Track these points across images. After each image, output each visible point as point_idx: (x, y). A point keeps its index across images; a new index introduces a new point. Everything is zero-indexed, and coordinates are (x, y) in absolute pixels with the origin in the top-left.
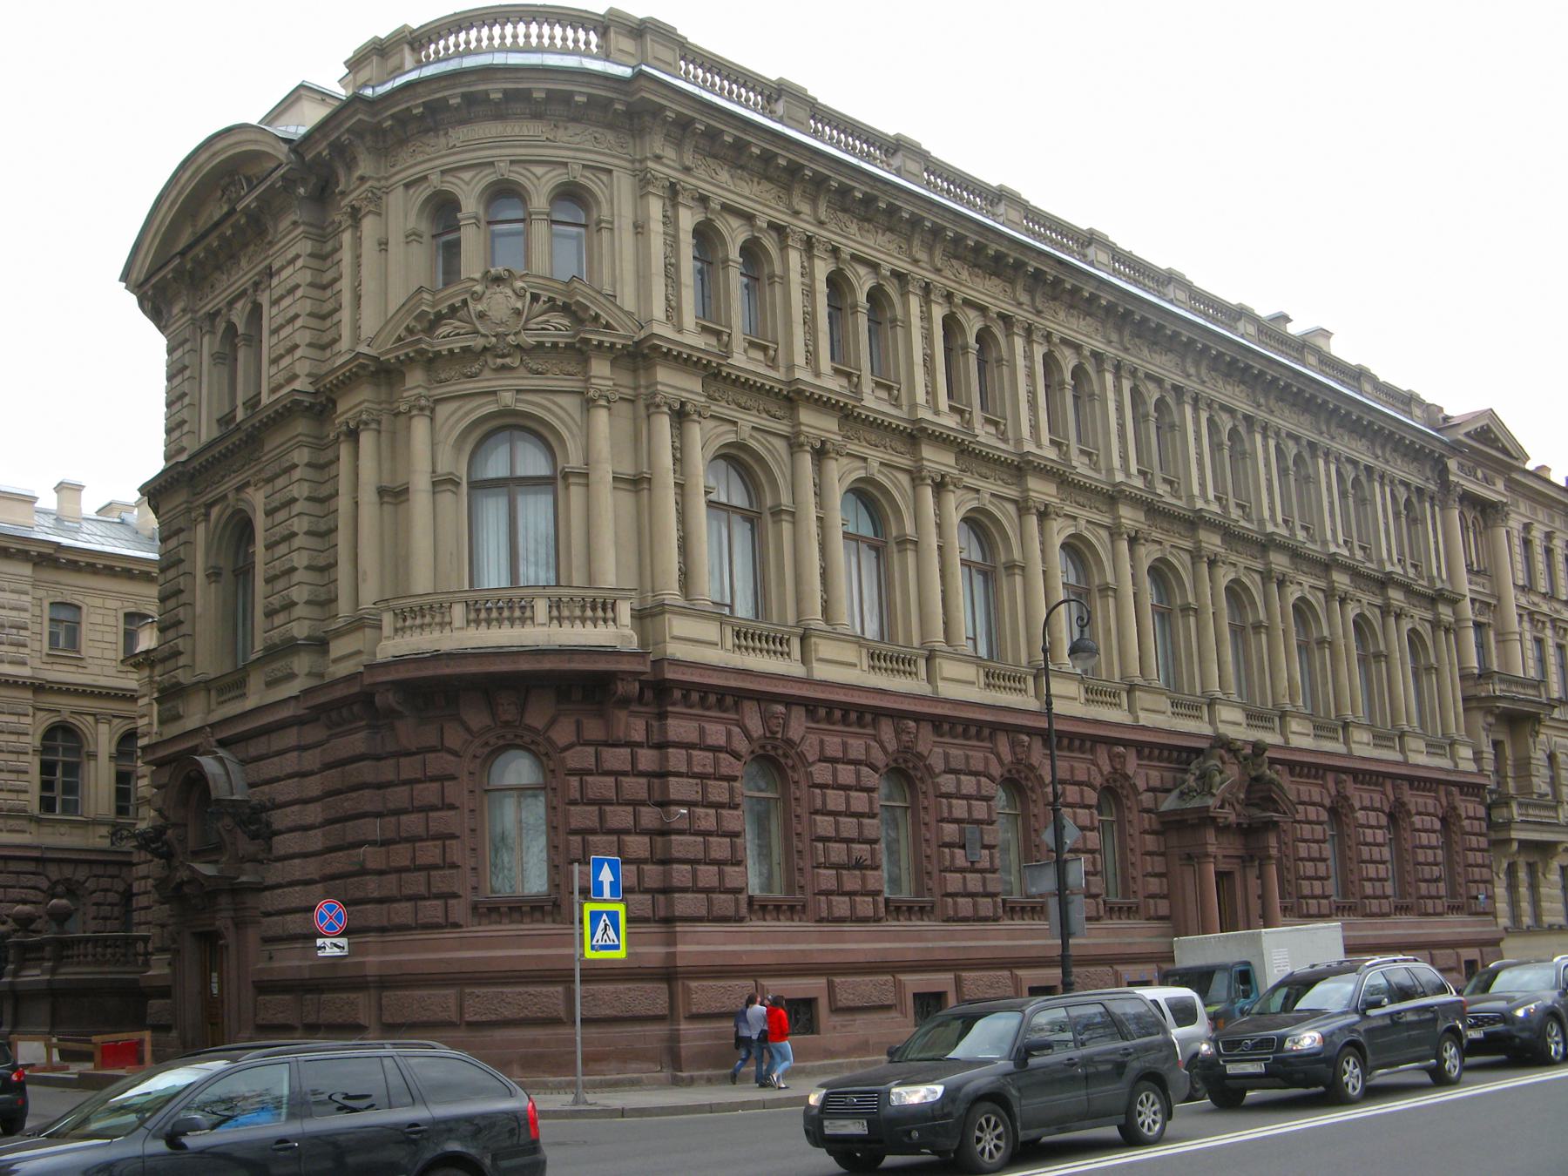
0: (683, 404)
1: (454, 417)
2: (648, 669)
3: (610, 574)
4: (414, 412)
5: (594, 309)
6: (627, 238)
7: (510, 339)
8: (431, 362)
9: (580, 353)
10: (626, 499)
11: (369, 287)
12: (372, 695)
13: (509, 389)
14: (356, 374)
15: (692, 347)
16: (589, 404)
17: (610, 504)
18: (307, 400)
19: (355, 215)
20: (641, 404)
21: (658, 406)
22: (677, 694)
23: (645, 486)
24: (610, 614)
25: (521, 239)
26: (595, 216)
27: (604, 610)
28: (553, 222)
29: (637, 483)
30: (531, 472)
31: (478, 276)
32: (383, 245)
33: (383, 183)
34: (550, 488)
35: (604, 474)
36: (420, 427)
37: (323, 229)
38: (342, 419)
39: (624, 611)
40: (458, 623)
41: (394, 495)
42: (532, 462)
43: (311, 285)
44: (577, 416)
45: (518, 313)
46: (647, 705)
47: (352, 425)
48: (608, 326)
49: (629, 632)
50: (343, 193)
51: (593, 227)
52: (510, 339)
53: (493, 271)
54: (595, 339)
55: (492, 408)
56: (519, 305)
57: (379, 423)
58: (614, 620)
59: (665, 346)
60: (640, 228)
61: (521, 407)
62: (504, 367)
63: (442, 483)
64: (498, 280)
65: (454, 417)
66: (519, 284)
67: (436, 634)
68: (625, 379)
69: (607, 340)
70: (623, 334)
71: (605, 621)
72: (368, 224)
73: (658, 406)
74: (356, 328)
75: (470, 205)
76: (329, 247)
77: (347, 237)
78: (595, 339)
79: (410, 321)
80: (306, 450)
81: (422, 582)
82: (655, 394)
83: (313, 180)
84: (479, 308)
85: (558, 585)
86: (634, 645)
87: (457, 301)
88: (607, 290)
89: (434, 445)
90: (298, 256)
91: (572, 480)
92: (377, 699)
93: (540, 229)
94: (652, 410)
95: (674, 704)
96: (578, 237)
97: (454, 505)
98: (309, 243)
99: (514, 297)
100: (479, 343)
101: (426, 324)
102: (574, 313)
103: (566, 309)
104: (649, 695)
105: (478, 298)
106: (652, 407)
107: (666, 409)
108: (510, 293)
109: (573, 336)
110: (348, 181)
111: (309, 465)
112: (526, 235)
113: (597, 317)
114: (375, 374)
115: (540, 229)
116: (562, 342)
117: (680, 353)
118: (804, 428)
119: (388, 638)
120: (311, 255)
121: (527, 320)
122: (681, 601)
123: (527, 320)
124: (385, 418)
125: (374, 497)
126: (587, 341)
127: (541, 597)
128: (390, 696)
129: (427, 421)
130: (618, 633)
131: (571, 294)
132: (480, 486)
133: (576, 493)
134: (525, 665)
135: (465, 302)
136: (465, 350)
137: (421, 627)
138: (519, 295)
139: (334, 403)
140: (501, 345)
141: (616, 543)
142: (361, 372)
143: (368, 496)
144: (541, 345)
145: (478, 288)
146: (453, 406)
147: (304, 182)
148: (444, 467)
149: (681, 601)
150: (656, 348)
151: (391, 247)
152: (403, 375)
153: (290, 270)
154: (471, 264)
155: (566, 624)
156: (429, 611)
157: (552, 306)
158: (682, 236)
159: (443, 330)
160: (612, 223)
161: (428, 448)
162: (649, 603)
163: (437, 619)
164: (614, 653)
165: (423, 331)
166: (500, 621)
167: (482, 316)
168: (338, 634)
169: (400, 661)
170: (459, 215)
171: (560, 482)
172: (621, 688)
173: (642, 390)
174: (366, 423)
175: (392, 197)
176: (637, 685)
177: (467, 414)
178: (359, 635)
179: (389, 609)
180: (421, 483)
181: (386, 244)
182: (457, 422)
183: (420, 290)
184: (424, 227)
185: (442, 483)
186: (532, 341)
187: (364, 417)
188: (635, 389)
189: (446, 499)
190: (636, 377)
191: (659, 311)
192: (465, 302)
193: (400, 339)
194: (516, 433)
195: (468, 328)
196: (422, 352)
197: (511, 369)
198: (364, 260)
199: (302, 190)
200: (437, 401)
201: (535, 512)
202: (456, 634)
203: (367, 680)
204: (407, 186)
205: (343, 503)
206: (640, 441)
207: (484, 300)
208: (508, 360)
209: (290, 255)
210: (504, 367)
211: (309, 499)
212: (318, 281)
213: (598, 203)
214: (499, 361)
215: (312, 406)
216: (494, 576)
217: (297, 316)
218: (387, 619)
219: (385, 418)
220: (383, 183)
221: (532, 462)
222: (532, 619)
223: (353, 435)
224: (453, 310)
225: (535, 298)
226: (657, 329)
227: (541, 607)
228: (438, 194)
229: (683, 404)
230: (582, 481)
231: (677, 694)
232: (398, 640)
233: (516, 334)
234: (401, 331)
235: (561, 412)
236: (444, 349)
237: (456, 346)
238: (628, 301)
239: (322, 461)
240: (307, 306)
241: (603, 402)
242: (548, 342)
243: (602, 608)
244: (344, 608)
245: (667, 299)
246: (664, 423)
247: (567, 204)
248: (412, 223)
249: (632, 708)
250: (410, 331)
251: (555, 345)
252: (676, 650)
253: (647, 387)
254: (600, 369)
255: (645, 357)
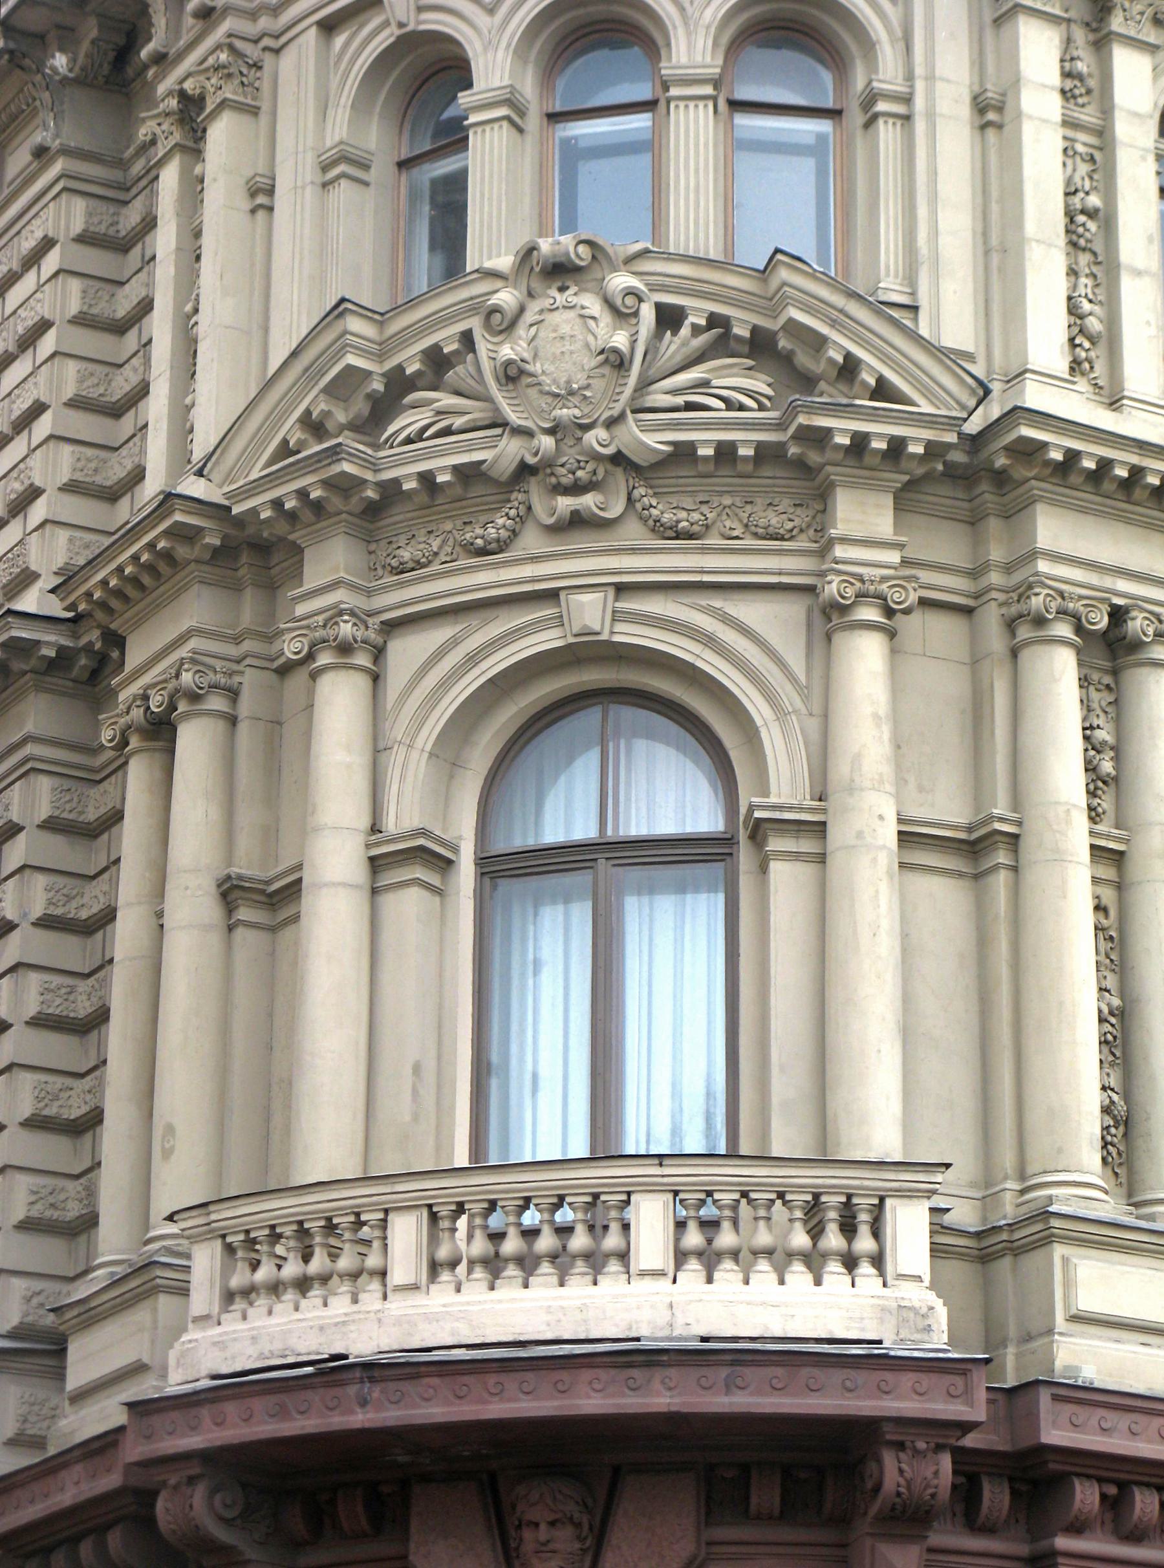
0: (1118, 615)
1: (436, 671)
2: (978, 1412)
3: (878, 1124)
4: (324, 659)
5: (841, 344)
6: (951, 144)
7: (595, 438)
8: (376, 512)
9: (802, 471)
10: (942, 897)
11: (218, 310)
12: (146, 1497)
13: (587, 585)
14: (168, 556)
15: (1142, 446)
16: (830, 619)
17: (879, 902)
18: (51, 640)
19: (192, 114)
20: (991, 617)
21: (1040, 621)
22: (1086, 1496)
23: (1002, 857)
24: (865, 1243)
25: (644, 161)
26: (860, 84)
27: (849, 1229)
28: (738, 105)
29: (979, 851)
30: (667, 826)
31: (504, 262)
32: (261, 194)
33: (264, 23)
34: (718, 869)
35: (871, 822)
36: (339, 701)
37: (122, 164)
38: (135, 688)
39: (909, 1229)
40: (399, 1275)
41: (263, 901)
42: (669, 796)
43: (82, 320)
44: (797, 664)
45: (617, 362)
46: (988, 1530)
47: (156, 702)
48: (882, 390)
49: (921, 1296)
50: (160, 58)
51: (855, 117)
52: (595, 438)
53: (545, 246)
54: (842, 429)
55: (548, 640)
56: (620, 340)
57: (233, 694)
58: (878, 1261)
59: (1057, 445)
60: (992, 112)
61: (629, 634)
62: (577, 521)
63: (400, 860)
64: (560, 271)
65: (436, 671)
66: (620, 281)
67: (340, 1305)
68: (942, 545)
69: (880, 432)
70: (929, 411)
71: (850, 1263)
72: (222, 135)
73: (1040, 621)
74: (182, 429)
75: (496, 64)
76: (132, 217)
77: (170, 178)
78: (842, 429)
79: (313, 401)
80: (44, 784)
81: (326, 1145)
82: (1025, 590)
83: (91, 30)
84: (507, 352)
85: (732, 1154)
86: (937, 1340)
87: (447, 338)
88: (892, 289)
89: (378, 751)
90: (47, 244)
91: (775, 844)
92: (160, 1505)
93: (694, 129)
94: (1024, 632)
95: (1077, 1528)
96: (817, 150)
97: (435, 928)
98: (79, 205)
99: (606, 319)
100: (507, 452)
101: (360, 407)
102: (786, 359)
103: (760, 347)
104: (995, 1497)
105: (503, 324)
106: (1024, 626)
107: (1064, 630)
108: (592, 304)
109: (781, 426)
110: (175, 28)
111: (50, 825)
112: (652, 147)
113: (849, 368)
114: (224, 554)
115: (694, 129)
116: (746, 442)
117: (1105, 465)
118: (1043, 566)
119: (203, 1320)
120: (84, 239)
121: (645, 384)
122: (1109, 1207)
123: (645, 384)
124: (250, 681)
125: (208, 908)
126: (820, 438)
127: (651, 1189)
128: (199, 1496)
129: (361, 682)
130: (884, 1302)
131: (774, 303)
132: (512, 870)
133: (787, 881)
134: (592, 1400)
135: (467, 338)
136: (468, 474)
137: (303, 1285)
138: (621, 312)
139: (117, 641)
140: (570, 456)
141: (908, 1034)
142: (182, 552)
143: (192, 905)
144: (683, 453)
145: (506, 298)
146: (439, 635)
147: (66, 37)
148: (405, 814)
149: (1109, 1207)
150: (1030, 451)
151: (282, 200)
152: (297, 551)
153: (28, 282)
154: (495, 235)
155: (727, 1273)
156: (325, 1240)
157: (720, 339)
158: (1123, 129)
159: (407, 422)
160: (908, 99)
161: (358, 760)
162: (1009, 1209)
163: (345, 1263)
164: (873, 1362)
165: (355, 427)
166: (527, 1264)
167: (513, 375)
168: (90, 1315)
169: (235, 1388)
170: (464, 99)
171: (745, 856)
172: (892, 1472)
173: (995, 578)
174: (194, 697)
175: (287, 61)
176: (946, 1462)
177: (472, 660)
178: (140, 1315)
179: (211, 1233)
180: (335, 861)
181: (270, 191)
182: (446, 684)
183: (340, 308)
184: (377, 139)
185: (400, 860)
186: (656, 442)
187: (187, 678)
188: (975, 573)
189: (408, 906)
190: (978, 542)
191: (1046, 340)
192: (467, 338)
193: (285, 450)
194: (628, 714)
195: (476, 411)
196: (344, 486)
197: (602, 524)
198: (208, 241)
199: (60, 61)
200: (392, 627)
201: (674, 945)
202: (398, 1305)
203: (134, 1451)
204: (329, 27)
205: (127, 933)
206: (989, 728)
207: (521, 331)
208: (589, 501)
209: (28, 243)
210: (577, 521)
211: (47, 923)
212: (101, 309)
213: (869, 46)
214: (565, 503)
215: (63, 660)
216: (549, 1124)
217: (38, 409)
218: (205, 1262)
219: (250, 681)
220: (264, 23)
221: (669, 796)
222: (623, 1256)
223: (161, 731)
224: (438, 363)
225: (669, 318)
226: (1036, 396)
227: (651, 1219)
228: (410, 42)
229: (1118, 615)
230: (806, 845)
231: (1086, 1496)
232: (232, 1325)
233: (612, 423)
234: (290, 429)
235: (745, 644)
236: (407, 474)
237: (442, 464)
238: (953, 319)
239: (91, 815)
240: (69, 379)
241: (869, 613)
242: (705, 442)
243: (841, 1223)
244: (113, 1243)
245: (1073, 309)
246: (1059, 673)
247: (787, 55)
248: (338, 128)
249: (936, 1539)
250: (315, 427)
251: (726, 452)
252: (1085, 1358)
253: (1008, 569)
254: (864, 518)
255: (1001, 479)
